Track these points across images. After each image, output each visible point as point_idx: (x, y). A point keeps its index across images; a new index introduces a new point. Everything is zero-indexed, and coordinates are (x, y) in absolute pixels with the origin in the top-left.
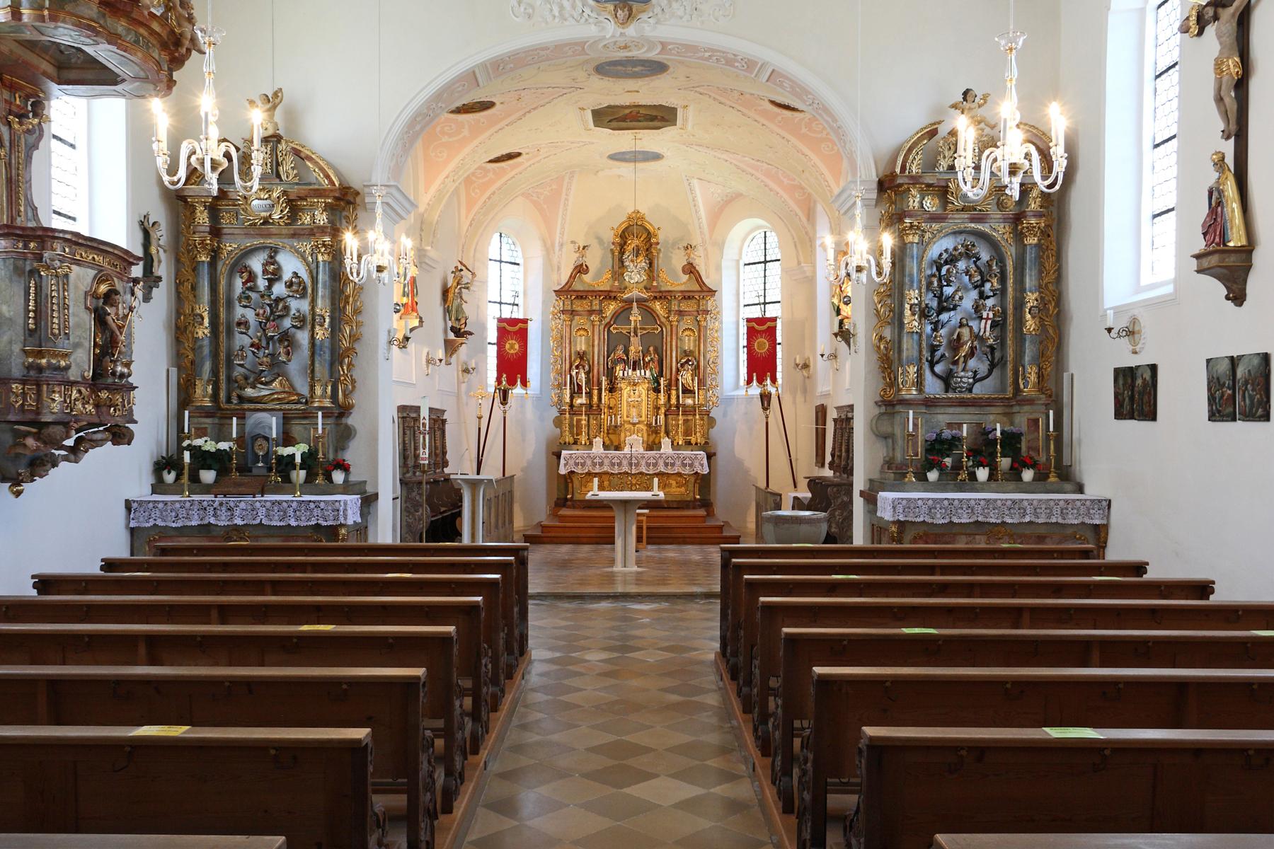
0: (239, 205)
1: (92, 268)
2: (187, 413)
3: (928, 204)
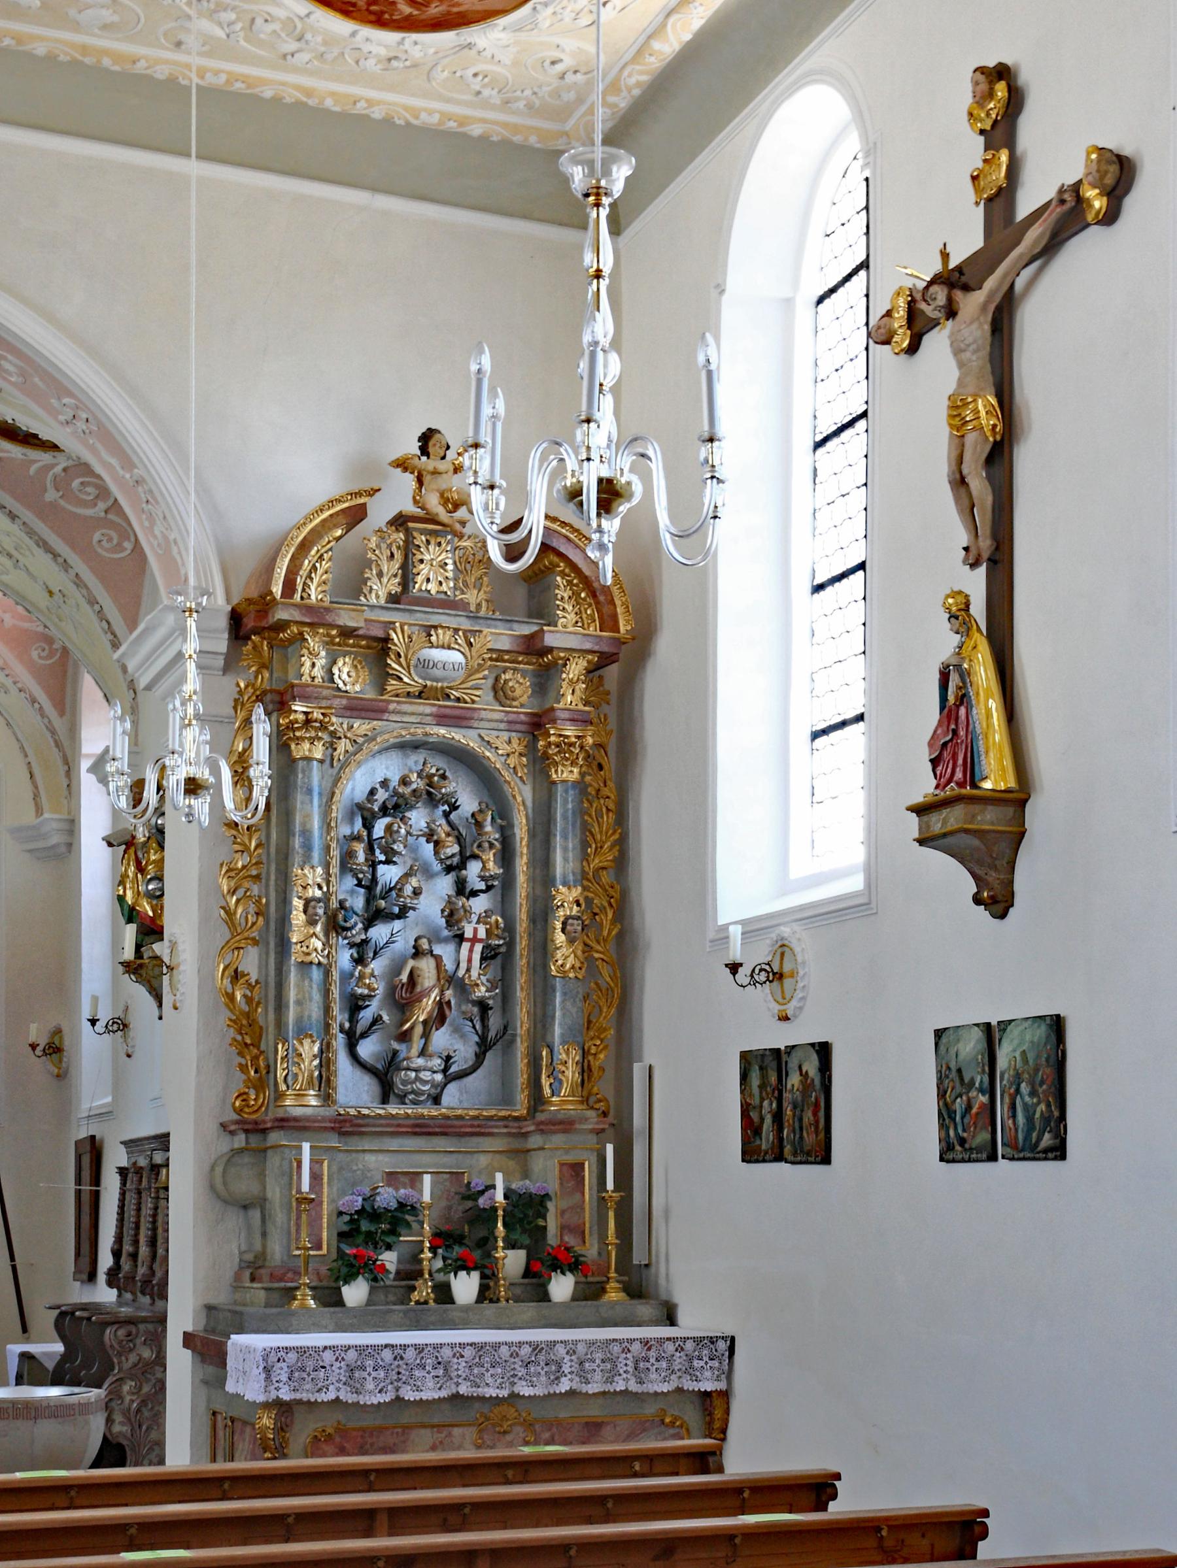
3: (345, 676)
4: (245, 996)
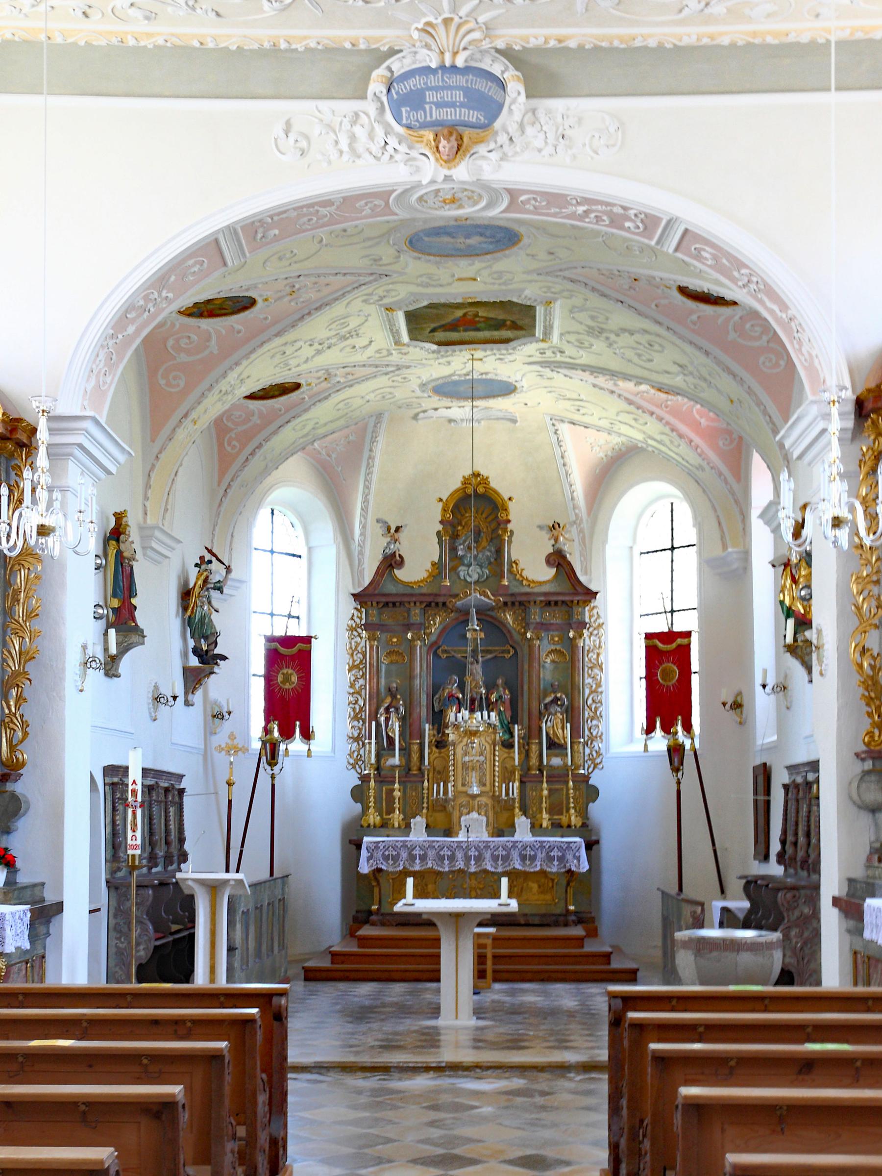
4: (870, 665)
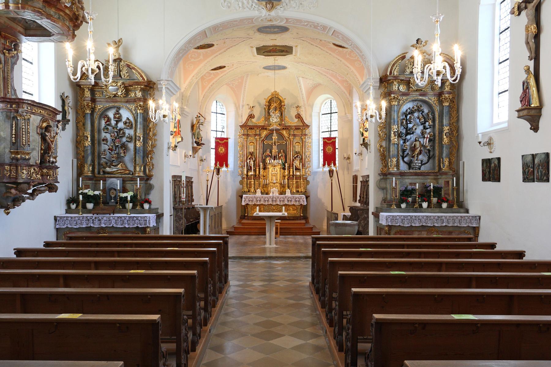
0: (103, 88)
1: (40, 116)
2: (81, 178)
3: (401, 88)
